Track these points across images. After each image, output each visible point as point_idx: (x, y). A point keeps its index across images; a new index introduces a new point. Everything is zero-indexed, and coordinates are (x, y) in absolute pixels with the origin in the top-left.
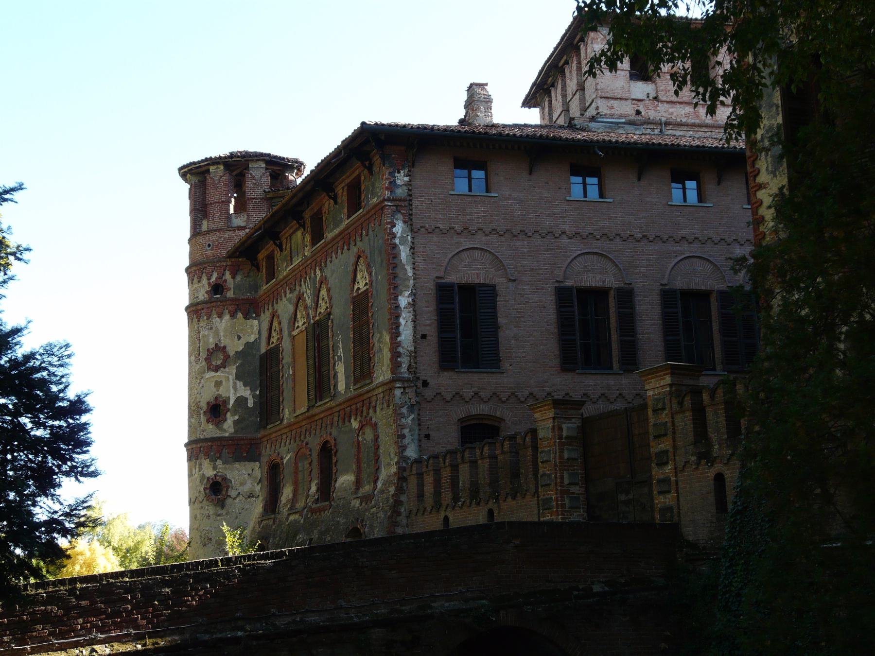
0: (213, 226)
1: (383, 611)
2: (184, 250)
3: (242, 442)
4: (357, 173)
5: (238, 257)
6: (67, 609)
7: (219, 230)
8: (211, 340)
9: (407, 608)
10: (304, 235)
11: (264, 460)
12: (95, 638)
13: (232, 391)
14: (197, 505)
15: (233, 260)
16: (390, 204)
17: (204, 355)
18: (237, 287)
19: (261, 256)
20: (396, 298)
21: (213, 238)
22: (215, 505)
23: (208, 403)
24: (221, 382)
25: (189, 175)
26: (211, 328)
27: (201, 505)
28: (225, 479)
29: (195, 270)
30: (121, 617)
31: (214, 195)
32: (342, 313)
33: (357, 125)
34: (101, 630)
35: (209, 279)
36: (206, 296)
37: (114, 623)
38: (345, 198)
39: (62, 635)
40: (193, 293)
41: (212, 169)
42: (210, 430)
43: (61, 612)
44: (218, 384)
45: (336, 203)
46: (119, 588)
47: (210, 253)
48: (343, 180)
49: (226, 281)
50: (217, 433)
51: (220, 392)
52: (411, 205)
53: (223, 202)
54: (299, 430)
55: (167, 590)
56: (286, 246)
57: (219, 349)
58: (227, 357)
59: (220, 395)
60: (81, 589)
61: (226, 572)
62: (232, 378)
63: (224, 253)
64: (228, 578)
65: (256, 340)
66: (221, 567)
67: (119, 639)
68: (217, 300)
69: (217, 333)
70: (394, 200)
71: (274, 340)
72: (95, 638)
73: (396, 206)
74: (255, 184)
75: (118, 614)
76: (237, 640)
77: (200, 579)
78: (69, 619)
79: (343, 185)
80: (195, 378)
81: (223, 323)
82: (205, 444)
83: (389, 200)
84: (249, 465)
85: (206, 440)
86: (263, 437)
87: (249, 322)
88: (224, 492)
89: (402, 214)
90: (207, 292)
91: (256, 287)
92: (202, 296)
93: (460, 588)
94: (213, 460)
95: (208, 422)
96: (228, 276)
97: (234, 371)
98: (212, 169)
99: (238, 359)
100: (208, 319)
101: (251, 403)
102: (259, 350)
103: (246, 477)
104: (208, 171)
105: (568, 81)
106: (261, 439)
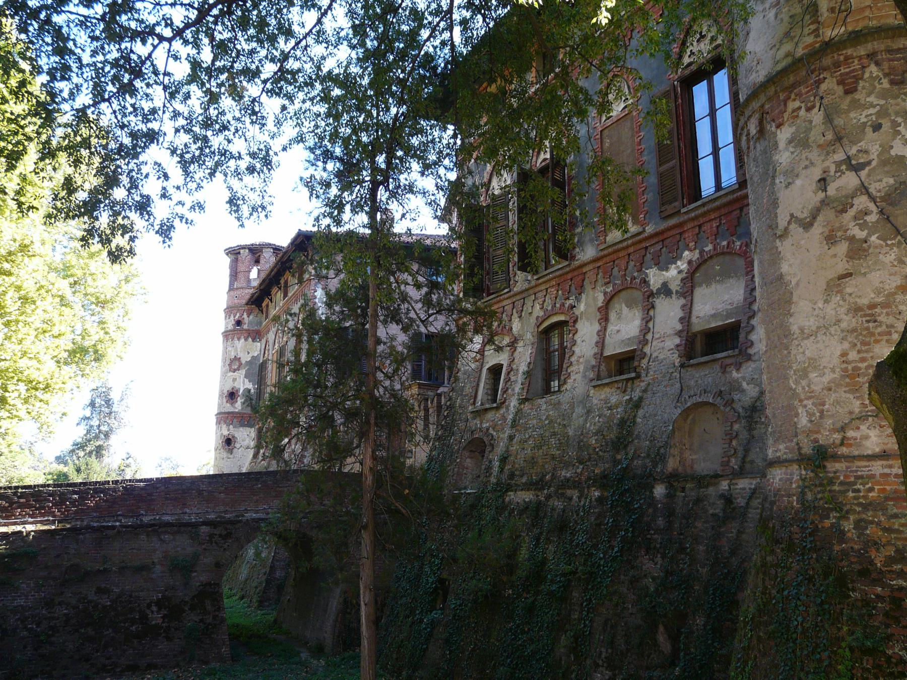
0: (239, 286)
1: (212, 516)
2: (224, 298)
6: (11, 503)
7: (242, 288)
9: (228, 516)
17: (228, 362)
18: (250, 323)
19: (264, 304)
21: (238, 292)
28: (233, 437)
29: (230, 310)
31: (241, 267)
33: (296, 231)
34: (32, 516)
39: (7, 518)
40: (227, 323)
41: (242, 251)
42: (228, 408)
43: (7, 505)
44: (234, 380)
47: (236, 301)
50: (232, 410)
57: (237, 359)
61: (114, 488)
62: (242, 376)
63: (244, 302)
67: (41, 522)
69: (236, 350)
75: (44, 508)
76: (113, 527)
77: (96, 491)
80: (224, 375)
81: (240, 344)
84: (248, 429)
85: (225, 413)
91: (261, 323)
92: (230, 327)
94: (228, 425)
96: (245, 316)
98: (242, 251)
104: (239, 253)
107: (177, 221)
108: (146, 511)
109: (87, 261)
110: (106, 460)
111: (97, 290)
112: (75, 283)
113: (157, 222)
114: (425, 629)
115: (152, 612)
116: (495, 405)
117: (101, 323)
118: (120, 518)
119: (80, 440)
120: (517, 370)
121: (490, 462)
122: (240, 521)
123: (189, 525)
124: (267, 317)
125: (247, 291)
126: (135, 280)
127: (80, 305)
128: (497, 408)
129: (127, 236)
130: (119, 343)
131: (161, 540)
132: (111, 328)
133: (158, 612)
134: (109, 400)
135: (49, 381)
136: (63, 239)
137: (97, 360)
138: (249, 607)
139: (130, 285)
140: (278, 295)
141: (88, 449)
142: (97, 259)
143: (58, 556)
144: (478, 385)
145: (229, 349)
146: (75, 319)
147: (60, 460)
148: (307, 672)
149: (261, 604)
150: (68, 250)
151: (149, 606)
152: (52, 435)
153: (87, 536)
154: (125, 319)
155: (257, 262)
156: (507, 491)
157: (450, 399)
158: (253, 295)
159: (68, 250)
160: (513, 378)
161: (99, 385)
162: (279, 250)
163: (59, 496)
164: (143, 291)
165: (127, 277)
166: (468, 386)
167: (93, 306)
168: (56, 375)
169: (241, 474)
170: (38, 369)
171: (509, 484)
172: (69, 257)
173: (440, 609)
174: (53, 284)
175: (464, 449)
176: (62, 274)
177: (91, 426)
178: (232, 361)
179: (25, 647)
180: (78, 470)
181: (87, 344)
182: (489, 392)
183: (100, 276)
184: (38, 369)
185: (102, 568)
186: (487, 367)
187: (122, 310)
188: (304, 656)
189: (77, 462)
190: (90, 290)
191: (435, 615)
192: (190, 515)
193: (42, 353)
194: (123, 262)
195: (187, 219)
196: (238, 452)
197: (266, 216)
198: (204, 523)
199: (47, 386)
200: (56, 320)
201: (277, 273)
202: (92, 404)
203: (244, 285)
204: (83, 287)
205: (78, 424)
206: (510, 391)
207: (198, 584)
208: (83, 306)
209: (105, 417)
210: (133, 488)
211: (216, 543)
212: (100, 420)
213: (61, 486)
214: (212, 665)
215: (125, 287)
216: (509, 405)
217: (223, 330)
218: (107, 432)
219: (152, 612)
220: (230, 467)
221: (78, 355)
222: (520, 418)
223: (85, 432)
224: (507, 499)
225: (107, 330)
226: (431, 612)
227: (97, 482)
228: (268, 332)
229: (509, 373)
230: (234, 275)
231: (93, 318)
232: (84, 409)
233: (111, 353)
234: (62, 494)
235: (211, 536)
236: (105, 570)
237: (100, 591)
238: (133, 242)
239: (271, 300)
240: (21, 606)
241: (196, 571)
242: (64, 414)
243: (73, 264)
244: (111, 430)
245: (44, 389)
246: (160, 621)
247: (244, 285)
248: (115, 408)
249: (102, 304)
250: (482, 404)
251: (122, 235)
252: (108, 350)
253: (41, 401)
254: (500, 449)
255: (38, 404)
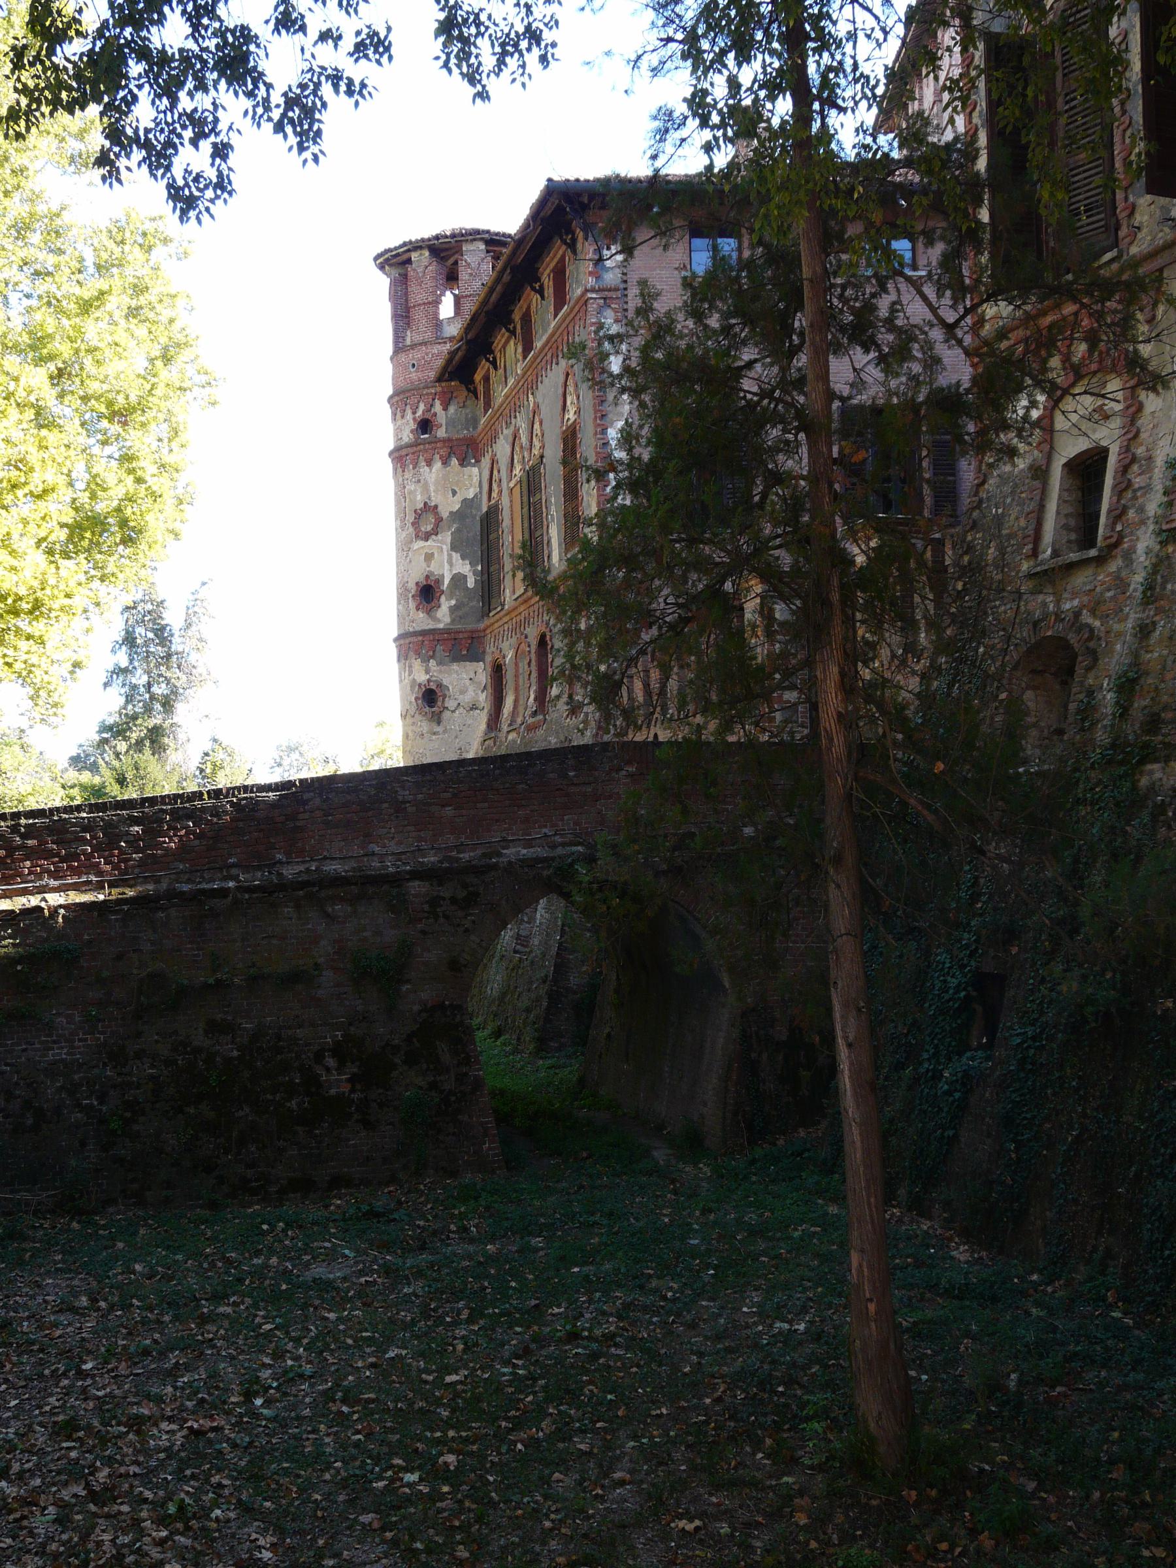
0: (418, 338)
1: (431, 859)
3: (461, 636)
4: (561, 252)
5: (451, 380)
7: (424, 343)
8: (419, 497)
9: (465, 856)
10: (516, 344)
11: (489, 658)
12: (47, 885)
13: (447, 566)
14: (409, 720)
15: (443, 384)
16: (594, 296)
17: (411, 518)
18: (450, 423)
19: (478, 377)
20: (604, 431)
21: (417, 354)
22: (431, 720)
23: (417, 584)
24: (433, 554)
25: (387, 268)
26: (419, 481)
27: (412, 720)
28: (440, 685)
29: (400, 399)
30: (79, 860)
31: (418, 295)
32: (554, 452)
33: (541, 185)
34: (55, 875)
35: (414, 413)
36: (411, 436)
37: (70, 867)
38: (551, 290)
40: (398, 431)
41: (414, 256)
42: (422, 622)
44: (429, 557)
45: (543, 298)
46: (74, 825)
47: (414, 375)
48: (548, 265)
49: (435, 414)
50: (430, 625)
51: (432, 569)
52: (626, 296)
53: (429, 303)
54: (518, 619)
55: (137, 828)
56: (500, 363)
57: (429, 509)
58: (439, 520)
59: (432, 573)
60: (26, 826)
61: (215, 807)
62: (446, 548)
63: (432, 375)
64: (217, 815)
65: (476, 496)
66: (207, 802)
67: (76, 887)
68: (424, 442)
70: (600, 290)
71: (494, 495)
72: (47, 885)
73: (605, 299)
74: (471, 274)
75: (75, 856)
76: (223, 893)
77: (179, 816)
78: (13, 862)
79: (548, 271)
80: (404, 548)
81: (433, 473)
82: (414, 639)
83: (593, 290)
84: (471, 667)
85: (415, 634)
86: (488, 627)
87: (467, 470)
88: (439, 703)
89: (614, 309)
90: (412, 431)
91: (475, 422)
92: (407, 437)
93: (544, 830)
94: (425, 660)
95: (418, 609)
96: (438, 407)
97: (449, 540)
98: (414, 256)
99: (454, 521)
100: (414, 468)
101: (471, 583)
102: (479, 508)
103: (468, 682)
104: (409, 261)
105: (925, 88)
106: (484, 630)
107: (326, 89)
108: (288, 854)
109: (77, 320)
110: (173, 757)
111: (106, 387)
112: (61, 373)
113: (277, 98)
114: (949, 1093)
115: (328, 1070)
116: (1093, 553)
117: (127, 458)
118: (234, 871)
119: (110, 721)
120: (1150, 459)
121: (1090, 693)
122: (495, 867)
123: (382, 879)
124: (488, 405)
125: (436, 349)
126: (186, 355)
127: (77, 422)
128: (1100, 560)
129: (206, 146)
130: (169, 501)
131: (328, 915)
132: (148, 467)
133: (340, 1069)
134: (163, 628)
135: (39, 594)
136: (19, 276)
137: (127, 541)
138: (515, 1051)
139: (174, 368)
140: (510, 351)
141: (134, 736)
142: (98, 314)
143: (120, 957)
144: (1042, 507)
145: (411, 487)
146: (72, 452)
147: (77, 762)
148: (675, 1192)
149: (542, 1045)
150: (34, 302)
151: (319, 1057)
152: (59, 711)
153: (173, 912)
154: (174, 445)
155: (452, 278)
156: (1143, 761)
157: (970, 549)
158: (452, 354)
159: (34, 302)
160: (1138, 481)
161: (139, 596)
162: (504, 244)
163: (103, 830)
164: (203, 379)
165: (166, 349)
166: (1014, 512)
167: (105, 423)
168: (52, 581)
169: (462, 763)
170: (14, 569)
171: (1146, 746)
172: (38, 316)
173: (981, 1047)
174: (16, 379)
175: (1015, 668)
176: (31, 354)
177: (134, 687)
178: (419, 515)
179: (83, 1144)
180: (121, 781)
181: (101, 507)
182: (1072, 522)
183: (108, 353)
184: (14, 569)
185: (211, 981)
186: (1064, 461)
187: (165, 426)
188: (661, 1155)
189: (116, 763)
190: (94, 387)
191: (971, 1061)
192: (382, 858)
193: (15, 536)
194: (205, 217)
195: (350, 82)
196: (454, 719)
197: (544, 59)
198: (415, 875)
199: (37, 605)
200: (34, 457)
201: (503, 295)
202: (129, 640)
203: (428, 335)
204: (77, 381)
205: (106, 685)
206: (1131, 514)
207: (416, 1008)
208: (83, 424)
209: (158, 665)
210: (254, 805)
211: (446, 917)
212: (148, 672)
213: (102, 807)
214: (468, 1178)
215: (165, 374)
216: (1132, 550)
217: (391, 446)
218: (166, 697)
219: (328, 1070)
220: (437, 751)
221: (88, 535)
222: (1165, 581)
223: (122, 700)
224: (1144, 782)
225: (139, 473)
226: (960, 1054)
227: (176, 796)
228: (494, 439)
229: (1124, 469)
230: (403, 315)
231: (108, 450)
232: (113, 651)
233: (155, 523)
234: (109, 826)
235: (434, 902)
236: (219, 982)
237: (215, 1028)
238: (225, 158)
239: (494, 364)
240: (62, 1060)
241: (408, 981)
242: (77, 665)
243: (50, 331)
244: (174, 692)
245: (31, 612)
246: (345, 1088)
247: (428, 335)
248: (177, 645)
249: (121, 415)
250: (1056, 554)
251: (194, 142)
252: (149, 517)
253: (29, 637)
254: (1116, 658)
255: (23, 645)
